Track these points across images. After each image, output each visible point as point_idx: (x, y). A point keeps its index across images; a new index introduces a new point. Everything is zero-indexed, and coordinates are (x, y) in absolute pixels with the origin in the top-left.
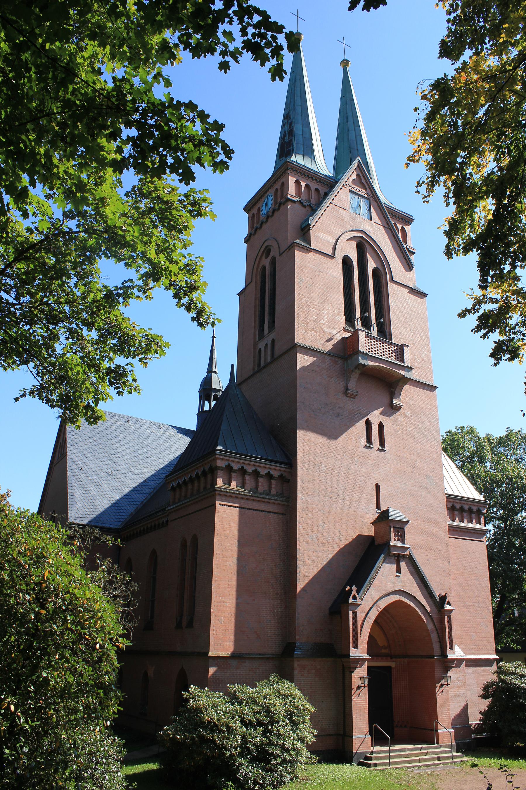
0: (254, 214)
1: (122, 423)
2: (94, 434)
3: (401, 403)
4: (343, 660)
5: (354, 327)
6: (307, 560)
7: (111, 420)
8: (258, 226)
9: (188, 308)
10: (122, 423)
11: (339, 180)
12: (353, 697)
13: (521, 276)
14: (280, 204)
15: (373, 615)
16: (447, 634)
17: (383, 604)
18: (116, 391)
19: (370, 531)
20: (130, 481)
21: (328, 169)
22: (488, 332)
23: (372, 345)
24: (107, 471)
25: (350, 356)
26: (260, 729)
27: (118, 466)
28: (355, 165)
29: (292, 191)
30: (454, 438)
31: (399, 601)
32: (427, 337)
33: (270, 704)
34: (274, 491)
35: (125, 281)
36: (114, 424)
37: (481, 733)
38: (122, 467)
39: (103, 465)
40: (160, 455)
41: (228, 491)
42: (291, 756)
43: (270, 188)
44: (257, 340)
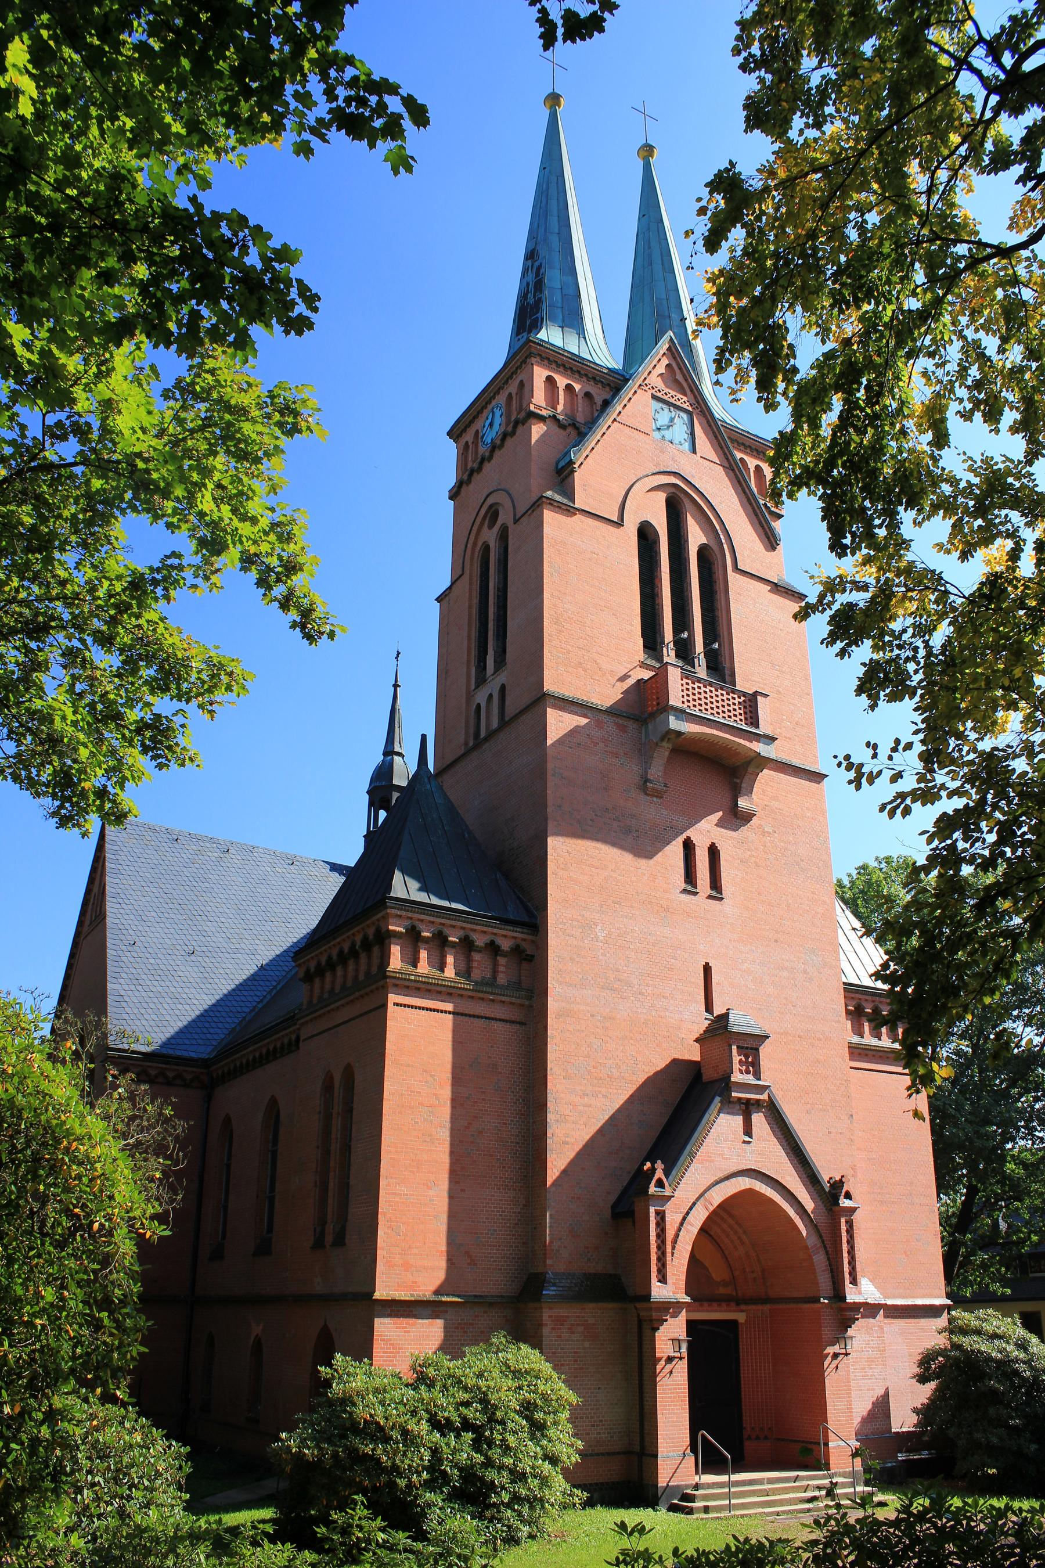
0: (467, 443)
1: (216, 855)
2: (161, 876)
3: (752, 807)
4: (638, 1305)
5: (659, 658)
6: (568, 1112)
7: (194, 848)
8: (476, 465)
9: (285, 604)
10: (216, 855)
11: (632, 375)
12: (658, 1379)
13: (912, 540)
14: (517, 423)
15: (698, 1218)
16: (845, 1255)
17: (718, 1196)
18: (154, 763)
19: (694, 1054)
20: (230, 966)
21: (611, 355)
22: (849, 645)
23: (694, 694)
24: (185, 948)
25: (652, 715)
26: (468, 1436)
27: (208, 939)
28: (663, 346)
29: (539, 398)
30: (870, 879)
31: (750, 1192)
32: (806, 678)
33: (489, 1387)
34: (502, 979)
35: (166, 556)
36: (201, 857)
37: (917, 1451)
38: (214, 939)
39: (177, 937)
40: (291, 916)
41: (412, 978)
42: (529, 1489)
43: (498, 392)
44: (473, 687)
